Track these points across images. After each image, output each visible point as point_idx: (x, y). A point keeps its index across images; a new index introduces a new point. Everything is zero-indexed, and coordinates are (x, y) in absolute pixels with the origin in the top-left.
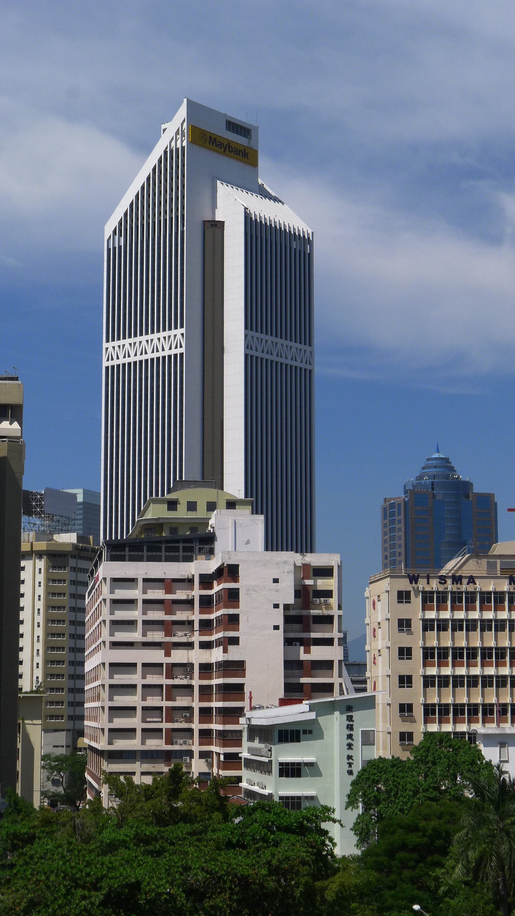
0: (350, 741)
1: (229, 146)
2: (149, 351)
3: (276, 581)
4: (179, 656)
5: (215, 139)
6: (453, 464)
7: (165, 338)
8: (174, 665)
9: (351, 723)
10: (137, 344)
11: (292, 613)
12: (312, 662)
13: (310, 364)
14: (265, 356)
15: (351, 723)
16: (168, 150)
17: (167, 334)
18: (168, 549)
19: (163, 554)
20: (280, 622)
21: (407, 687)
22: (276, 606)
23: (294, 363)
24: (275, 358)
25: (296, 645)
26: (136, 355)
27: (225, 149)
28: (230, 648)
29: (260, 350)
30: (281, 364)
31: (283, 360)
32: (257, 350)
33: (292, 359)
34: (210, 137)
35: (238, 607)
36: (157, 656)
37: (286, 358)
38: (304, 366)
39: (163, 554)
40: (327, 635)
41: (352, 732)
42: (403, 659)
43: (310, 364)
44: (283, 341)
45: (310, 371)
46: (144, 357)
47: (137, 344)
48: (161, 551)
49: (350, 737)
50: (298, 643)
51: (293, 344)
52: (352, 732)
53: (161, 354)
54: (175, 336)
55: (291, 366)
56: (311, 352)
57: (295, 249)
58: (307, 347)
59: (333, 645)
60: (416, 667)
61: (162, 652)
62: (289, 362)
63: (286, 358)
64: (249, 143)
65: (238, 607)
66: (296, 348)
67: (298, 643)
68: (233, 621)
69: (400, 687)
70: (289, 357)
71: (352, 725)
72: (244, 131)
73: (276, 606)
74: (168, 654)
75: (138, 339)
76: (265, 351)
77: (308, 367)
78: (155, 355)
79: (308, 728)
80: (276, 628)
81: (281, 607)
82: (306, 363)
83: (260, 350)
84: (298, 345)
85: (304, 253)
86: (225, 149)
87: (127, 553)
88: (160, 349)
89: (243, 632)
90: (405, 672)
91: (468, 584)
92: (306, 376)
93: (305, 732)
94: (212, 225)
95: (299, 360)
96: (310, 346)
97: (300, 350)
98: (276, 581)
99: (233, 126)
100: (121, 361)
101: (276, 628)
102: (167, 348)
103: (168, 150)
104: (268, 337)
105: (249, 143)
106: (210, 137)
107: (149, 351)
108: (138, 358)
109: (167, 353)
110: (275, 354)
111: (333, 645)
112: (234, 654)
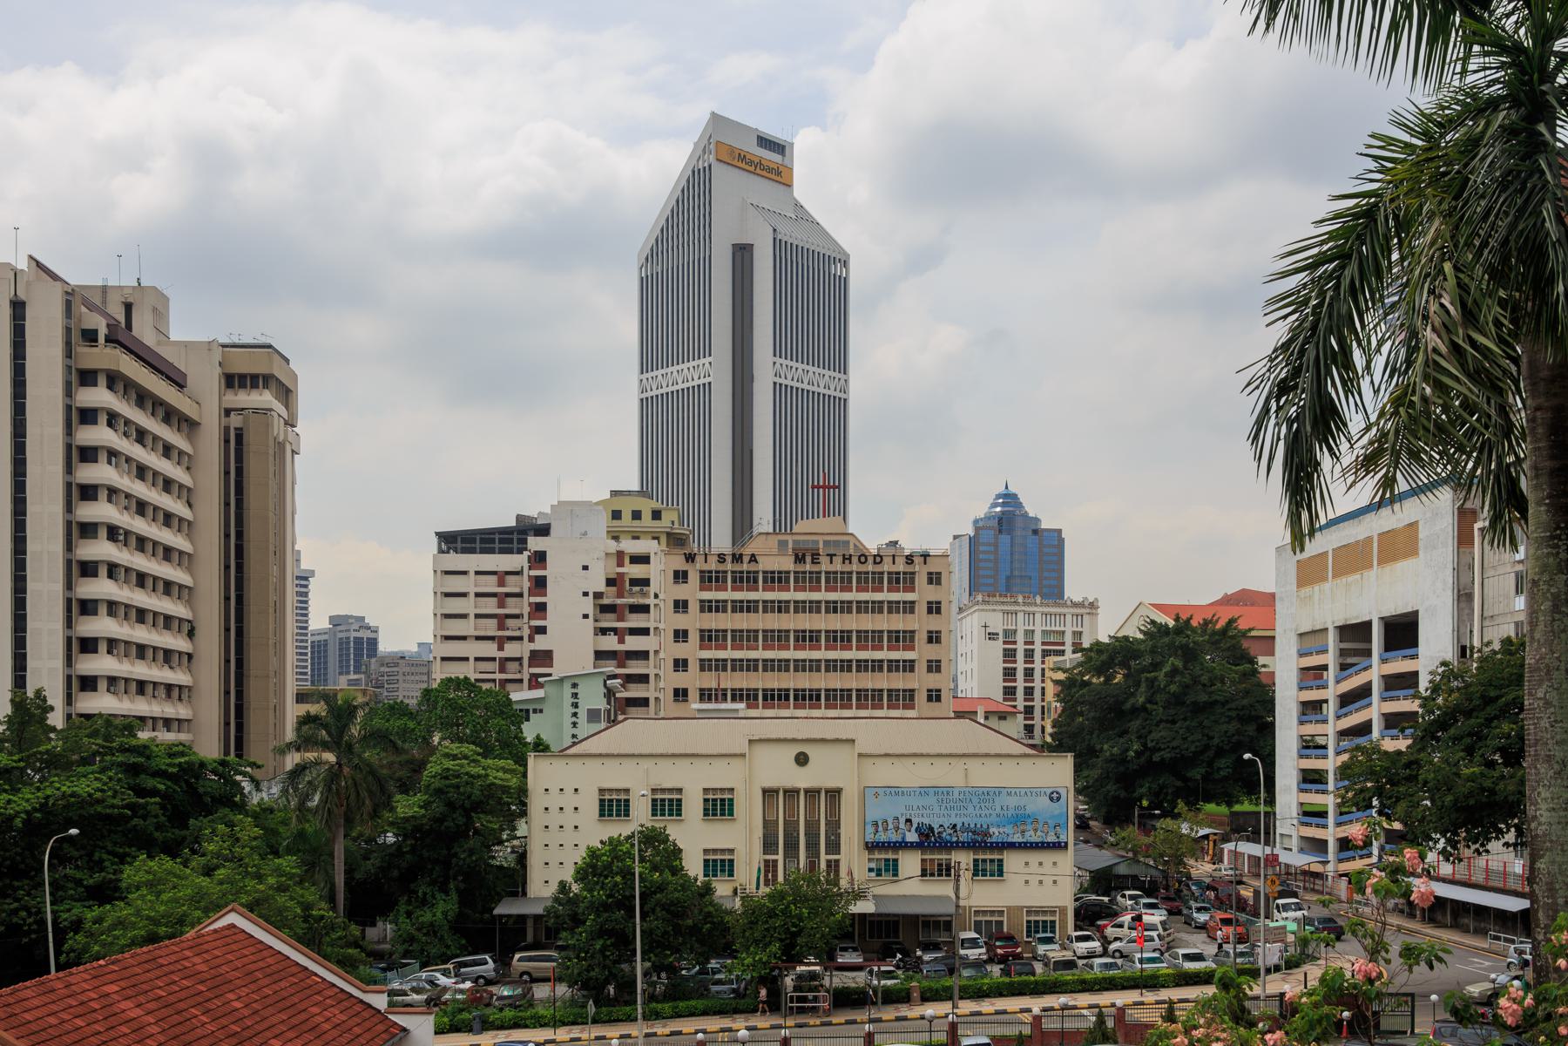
3: (585, 568)
4: (511, 650)
11: (606, 601)
17: (695, 363)
18: (501, 541)
19: (497, 545)
20: (590, 611)
22: (586, 594)
23: (827, 392)
36: (490, 649)
38: (838, 394)
39: (497, 545)
40: (643, 625)
46: (675, 388)
49: (575, 715)
51: (826, 372)
53: (690, 384)
60: (691, 650)
61: (495, 646)
68: (540, 609)
72: (779, 147)
73: (586, 594)
74: (501, 648)
75: (670, 369)
77: (843, 396)
78: (685, 386)
79: (538, 707)
80: (586, 616)
87: (459, 545)
90: (681, 656)
92: (840, 405)
93: (535, 711)
98: (585, 568)
99: (765, 142)
100: (654, 393)
101: (586, 616)
104: (799, 365)
108: (670, 389)
112: (541, 643)
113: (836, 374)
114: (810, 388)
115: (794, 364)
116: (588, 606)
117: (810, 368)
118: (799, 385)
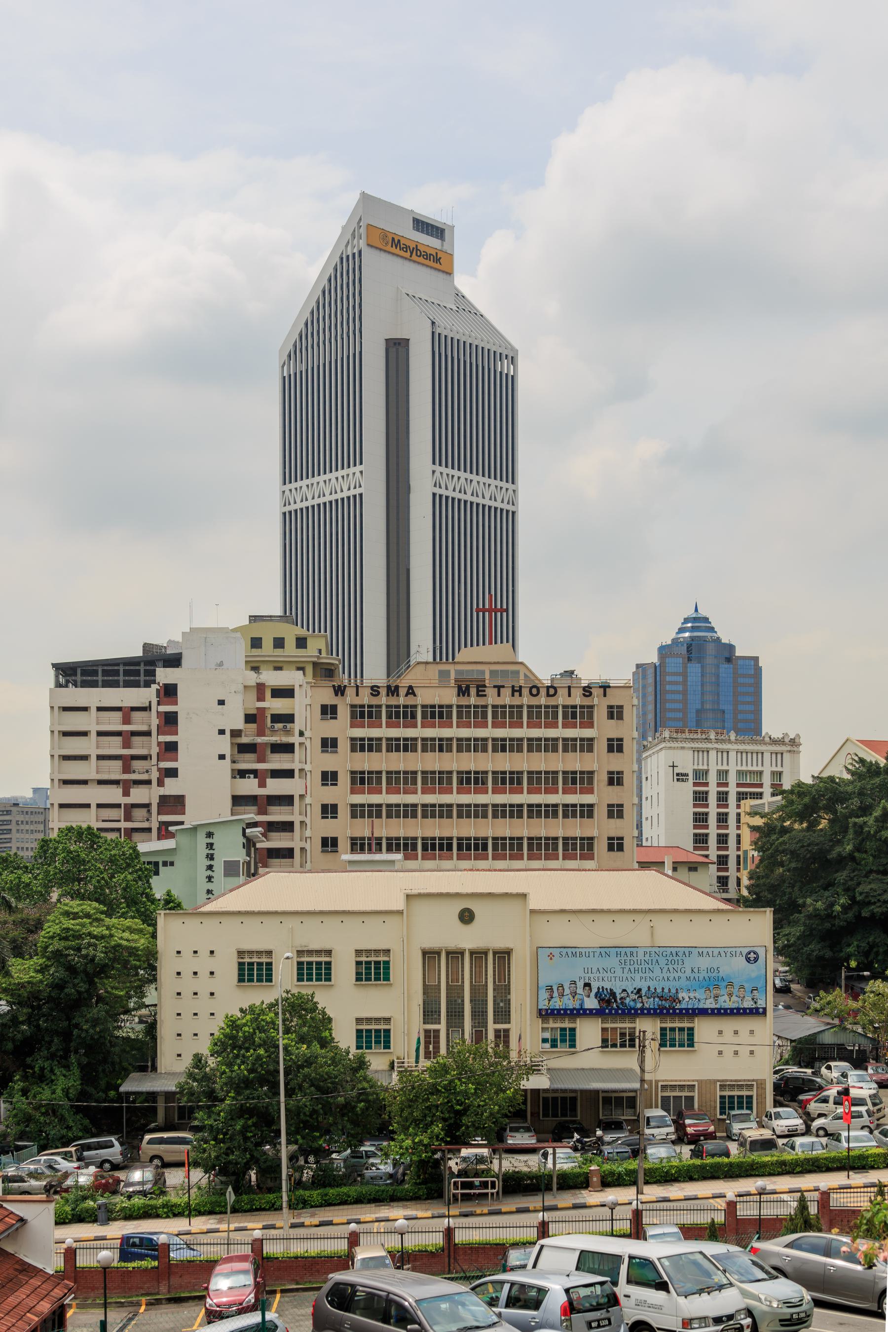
0: (209, 873)
1: (417, 250)
2: (304, 488)
3: (221, 702)
4: (138, 795)
5: (399, 241)
6: (713, 625)
7: (343, 477)
8: (134, 806)
9: (211, 852)
10: (315, 485)
11: (244, 740)
12: (268, 796)
13: (513, 504)
14: (457, 495)
15: (211, 852)
16: (344, 256)
18: (126, 673)
19: (121, 678)
20: (227, 750)
21: (332, 817)
22: (222, 732)
23: (493, 504)
24: (469, 498)
25: (249, 777)
26: (313, 498)
27: (412, 253)
28: (167, 781)
29: (451, 488)
30: (478, 505)
31: (480, 500)
32: (447, 489)
33: (491, 499)
34: (393, 239)
35: (177, 734)
36: (114, 794)
37: (483, 497)
38: (505, 506)
40: (286, 766)
41: (212, 863)
42: (327, 785)
43: (513, 504)
44: (480, 478)
45: (513, 513)
46: (321, 500)
47: (315, 485)
48: (119, 675)
49: (210, 867)
50: (252, 776)
51: (492, 481)
52: (212, 863)
53: (339, 496)
54: (354, 474)
55: (490, 507)
56: (514, 491)
57: (512, 377)
58: (509, 485)
59: (293, 777)
60: (342, 795)
62: (487, 502)
63: (483, 497)
64: (442, 245)
65: (177, 734)
66: (466, 479)
67: (252, 776)
69: (323, 818)
70: (487, 496)
71: (212, 855)
72: (437, 231)
73: (222, 732)
74: (126, 793)
76: (457, 490)
77: (510, 508)
80: (222, 757)
81: (228, 733)
82: (508, 503)
83: (451, 488)
84: (498, 482)
85: (495, 371)
86: (412, 253)
88: (338, 490)
89: (181, 763)
91: (406, 695)
93: (165, 864)
94: (395, 344)
95: (499, 499)
96: (513, 483)
97: (501, 488)
98: (221, 702)
99: (422, 225)
100: (299, 505)
101: (222, 757)
102: (345, 488)
103: (344, 256)
104: (461, 473)
105: (442, 245)
106: (393, 239)
107: (327, 493)
108: (316, 501)
109: (345, 494)
110: (469, 492)
111: (293, 777)
112: (171, 787)
113: (503, 484)
114: (475, 500)
115: (455, 472)
116: (225, 745)
117: (473, 477)
118: (462, 497)
